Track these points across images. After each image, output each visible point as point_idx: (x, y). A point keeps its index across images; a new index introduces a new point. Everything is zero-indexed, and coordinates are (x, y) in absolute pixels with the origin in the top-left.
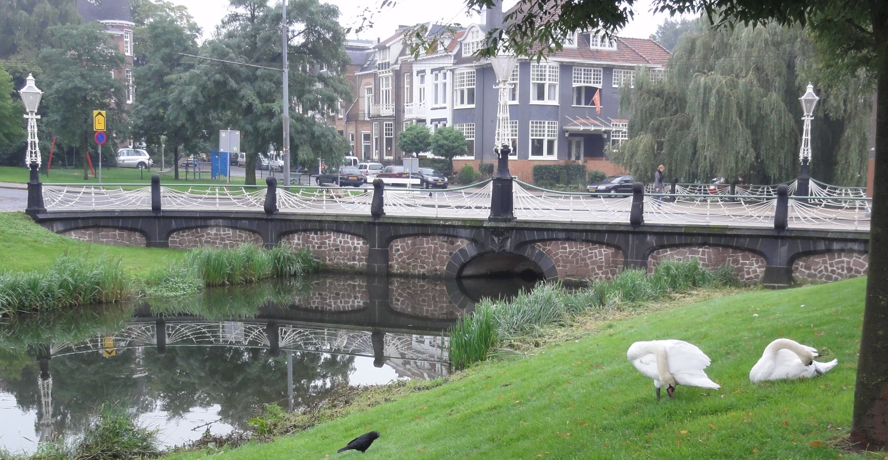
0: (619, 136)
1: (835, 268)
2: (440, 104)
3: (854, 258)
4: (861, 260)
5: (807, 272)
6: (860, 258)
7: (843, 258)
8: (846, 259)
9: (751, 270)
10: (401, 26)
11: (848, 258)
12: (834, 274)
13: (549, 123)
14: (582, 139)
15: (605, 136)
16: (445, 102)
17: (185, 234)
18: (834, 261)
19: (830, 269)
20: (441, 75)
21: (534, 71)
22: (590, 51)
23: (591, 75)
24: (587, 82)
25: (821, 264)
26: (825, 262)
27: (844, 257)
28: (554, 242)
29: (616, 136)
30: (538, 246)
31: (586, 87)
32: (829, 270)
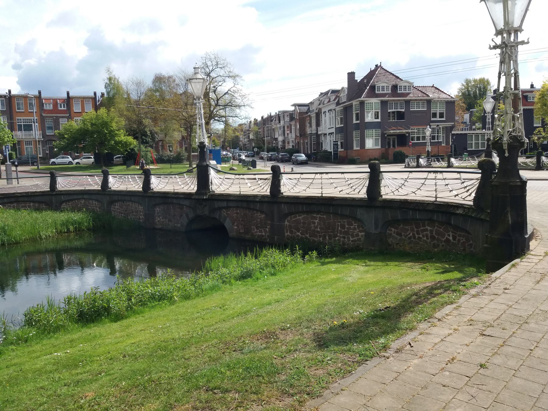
0: (415, 134)
1: (421, 236)
2: (332, 126)
3: (436, 227)
4: (441, 230)
5: (399, 237)
6: (440, 228)
7: (427, 227)
8: (429, 228)
9: (354, 234)
10: (321, 93)
11: (430, 227)
12: (421, 241)
13: (375, 130)
14: (395, 137)
15: (407, 135)
16: (333, 125)
17: (70, 203)
18: (419, 229)
19: (417, 236)
20: (331, 113)
21: (389, 105)
22: (398, 93)
23: (415, 105)
24: (396, 109)
25: (409, 231)
26: (412, 230)
27: (428, 226)
28: (231, 209)
29: (413, 135)
30: (224, 211)
31: (397, 111)
32: (417, 237)
